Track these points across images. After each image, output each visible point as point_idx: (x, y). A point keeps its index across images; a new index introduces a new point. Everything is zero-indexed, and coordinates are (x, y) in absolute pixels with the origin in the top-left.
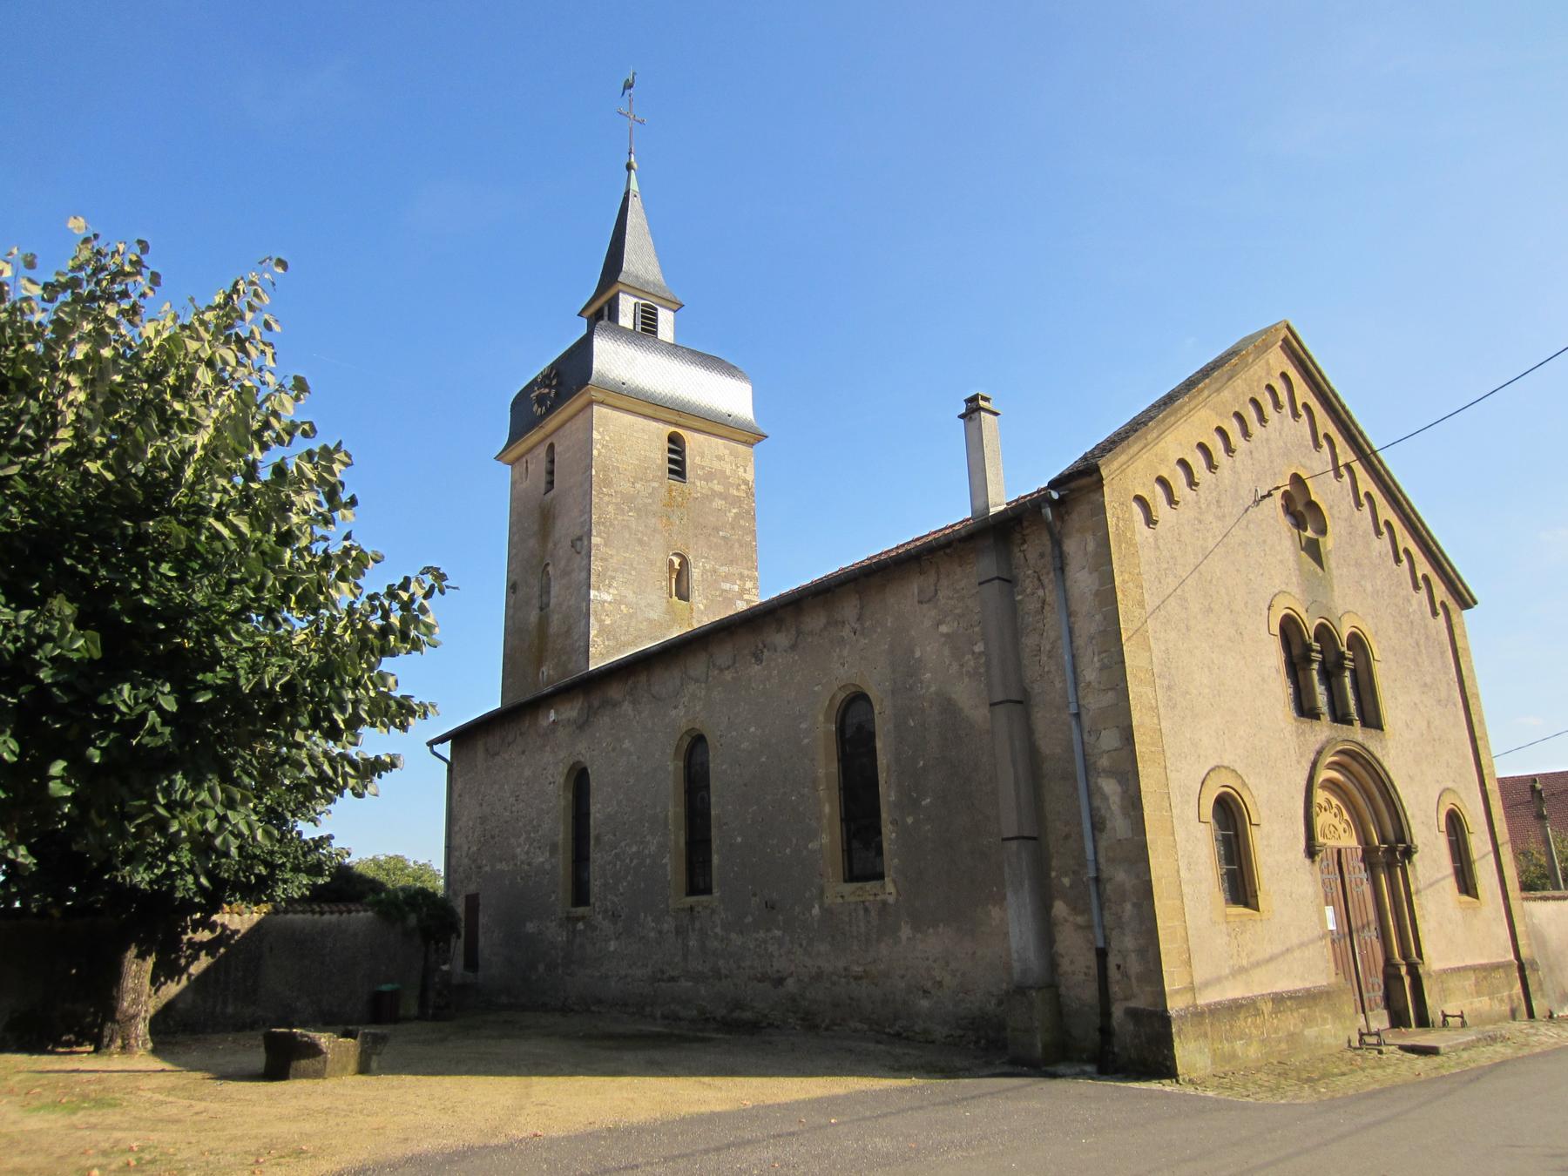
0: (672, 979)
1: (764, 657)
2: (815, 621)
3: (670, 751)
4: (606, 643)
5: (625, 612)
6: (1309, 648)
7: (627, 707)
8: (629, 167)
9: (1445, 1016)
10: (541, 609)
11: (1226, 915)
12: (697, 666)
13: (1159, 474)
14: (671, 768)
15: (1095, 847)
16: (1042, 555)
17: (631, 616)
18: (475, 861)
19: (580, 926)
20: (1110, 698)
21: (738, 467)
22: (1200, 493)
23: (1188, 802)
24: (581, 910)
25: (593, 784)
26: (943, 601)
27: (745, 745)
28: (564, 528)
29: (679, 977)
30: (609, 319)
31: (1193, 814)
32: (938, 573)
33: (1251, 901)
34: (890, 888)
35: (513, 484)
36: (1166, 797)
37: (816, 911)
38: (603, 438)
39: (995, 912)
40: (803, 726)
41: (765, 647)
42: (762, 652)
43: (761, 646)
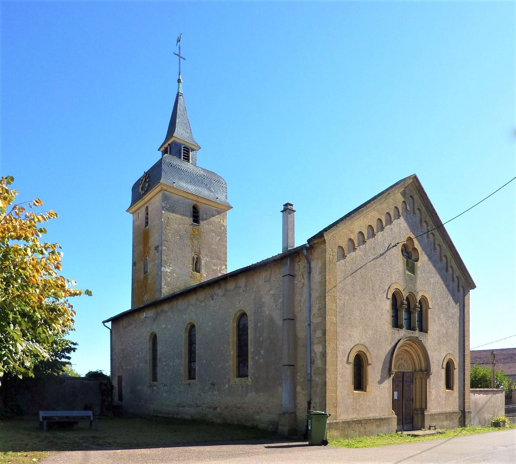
0: (183, 406)
1: (215, 298)
3: (184, 330)
4: (168, 288)
5: (175, 276)
6: (402, 304)
7: (169, 313)
8: (179, 81)
9: (430, 426)
10: (145, 273)
11: (446, 391)
12: (192, 299)
13: (350, 238)
14: (184, 336)
15: (311, 369)
16: (304, 267)
17: (178, 278)
19: (155, 388)
20: (319, 320)
21: (221, 220)
22: (367, 245)
23: (344, 356)
24: (155, 383)
25: (158, 340)
28: (153, 240)
29: (185, 406)
30: (170, 154)
32: (271, 271)
33: (364, 389)
34: (250, 380)
35: (134, 222)
36: (336, 354)
37: (227, 386)
38: (166, 206)
40: (226, 324)
41: (215, 294)
42: (214, 296)
43: (213, 294)
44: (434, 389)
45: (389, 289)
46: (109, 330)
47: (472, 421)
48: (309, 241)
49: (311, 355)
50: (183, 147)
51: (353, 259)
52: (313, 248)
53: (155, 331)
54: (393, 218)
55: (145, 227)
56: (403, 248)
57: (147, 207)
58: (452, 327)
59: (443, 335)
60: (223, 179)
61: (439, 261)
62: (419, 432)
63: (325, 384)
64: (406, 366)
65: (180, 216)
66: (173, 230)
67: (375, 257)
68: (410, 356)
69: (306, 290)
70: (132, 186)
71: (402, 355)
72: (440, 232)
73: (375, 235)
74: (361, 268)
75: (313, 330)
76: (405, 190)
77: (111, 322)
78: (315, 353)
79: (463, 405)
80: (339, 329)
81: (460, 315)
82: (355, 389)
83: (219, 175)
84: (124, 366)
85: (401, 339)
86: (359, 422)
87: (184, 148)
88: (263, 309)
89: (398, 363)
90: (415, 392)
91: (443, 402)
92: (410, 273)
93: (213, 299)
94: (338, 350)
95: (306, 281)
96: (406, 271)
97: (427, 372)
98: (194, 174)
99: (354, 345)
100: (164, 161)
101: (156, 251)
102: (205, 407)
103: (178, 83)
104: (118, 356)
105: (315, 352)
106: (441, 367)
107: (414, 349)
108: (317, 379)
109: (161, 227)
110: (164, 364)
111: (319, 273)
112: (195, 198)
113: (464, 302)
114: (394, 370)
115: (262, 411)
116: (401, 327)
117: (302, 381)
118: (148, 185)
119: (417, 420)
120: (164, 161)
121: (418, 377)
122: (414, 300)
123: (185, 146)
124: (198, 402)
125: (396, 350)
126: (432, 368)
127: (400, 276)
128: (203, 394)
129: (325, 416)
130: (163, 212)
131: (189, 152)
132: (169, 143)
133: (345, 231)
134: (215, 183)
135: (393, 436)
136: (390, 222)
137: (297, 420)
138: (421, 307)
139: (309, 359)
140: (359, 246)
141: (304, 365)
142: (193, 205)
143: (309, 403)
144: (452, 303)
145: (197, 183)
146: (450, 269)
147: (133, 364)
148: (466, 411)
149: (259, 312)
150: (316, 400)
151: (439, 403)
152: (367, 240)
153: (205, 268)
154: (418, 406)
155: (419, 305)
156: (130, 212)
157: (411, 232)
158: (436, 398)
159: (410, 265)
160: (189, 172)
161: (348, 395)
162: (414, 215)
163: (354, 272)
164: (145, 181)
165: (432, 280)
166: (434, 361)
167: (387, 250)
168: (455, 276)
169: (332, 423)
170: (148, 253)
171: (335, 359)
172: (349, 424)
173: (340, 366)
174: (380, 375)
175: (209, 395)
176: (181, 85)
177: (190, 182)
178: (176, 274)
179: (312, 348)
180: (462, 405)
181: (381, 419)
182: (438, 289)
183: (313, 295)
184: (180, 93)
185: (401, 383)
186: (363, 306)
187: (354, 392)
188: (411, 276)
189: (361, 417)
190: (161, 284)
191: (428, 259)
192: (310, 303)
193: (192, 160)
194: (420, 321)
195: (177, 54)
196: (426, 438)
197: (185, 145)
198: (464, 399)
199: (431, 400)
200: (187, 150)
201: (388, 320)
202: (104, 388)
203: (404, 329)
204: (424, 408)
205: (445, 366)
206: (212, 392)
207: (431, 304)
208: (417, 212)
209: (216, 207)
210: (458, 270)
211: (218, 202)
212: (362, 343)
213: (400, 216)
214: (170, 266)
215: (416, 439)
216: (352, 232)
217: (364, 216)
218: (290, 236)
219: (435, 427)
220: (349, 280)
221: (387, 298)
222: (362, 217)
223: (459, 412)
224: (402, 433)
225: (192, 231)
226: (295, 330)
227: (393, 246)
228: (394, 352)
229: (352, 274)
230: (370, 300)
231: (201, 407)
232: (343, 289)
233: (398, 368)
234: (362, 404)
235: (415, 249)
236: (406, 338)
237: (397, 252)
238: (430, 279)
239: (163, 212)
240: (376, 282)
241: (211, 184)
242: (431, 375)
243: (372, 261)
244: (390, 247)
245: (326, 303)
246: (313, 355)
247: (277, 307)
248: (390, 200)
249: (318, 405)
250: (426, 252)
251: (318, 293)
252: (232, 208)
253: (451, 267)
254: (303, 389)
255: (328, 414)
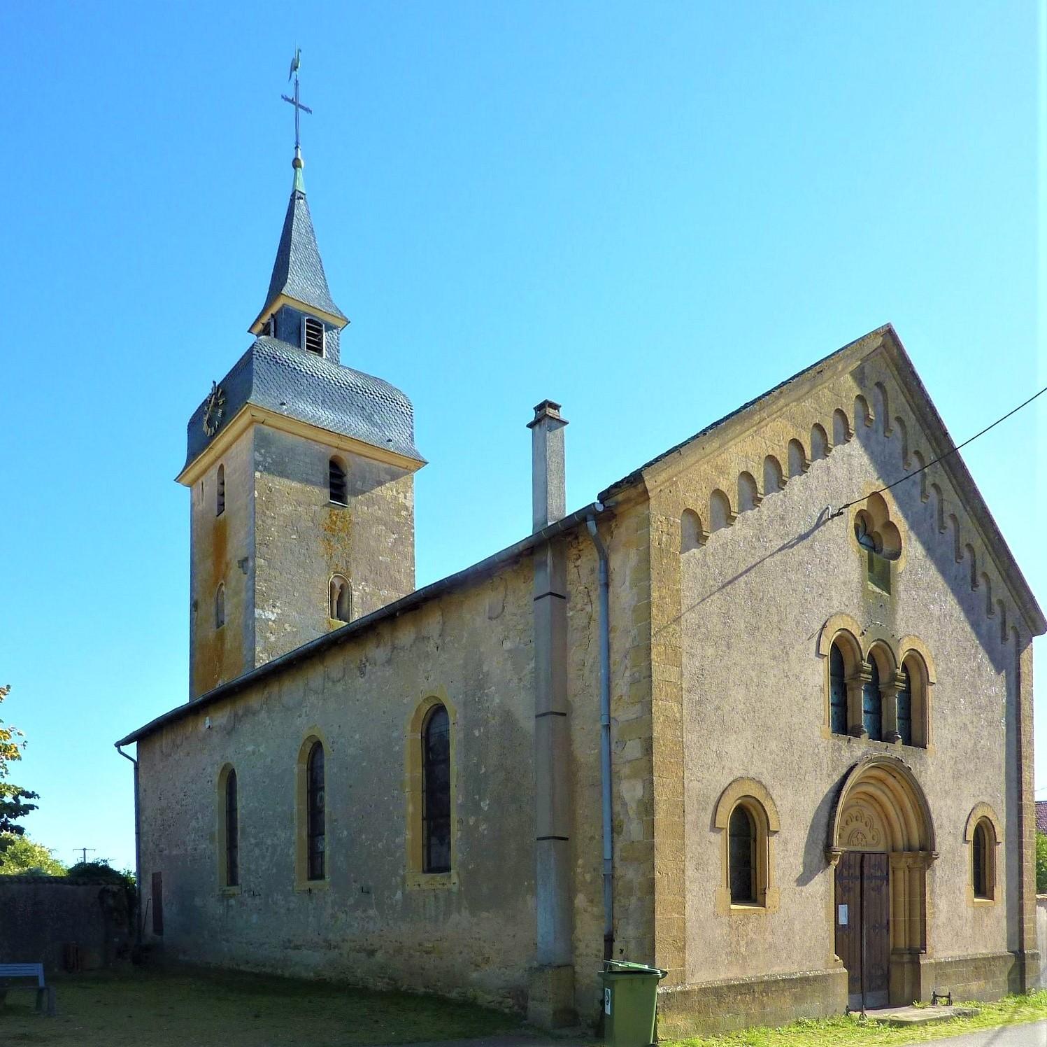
0: (297, 947)
2: (406, 635)
3: (296, 755)
6: (858, 669)
7: (263, 715)
8: (296, 164)
9: (935, 996)
11: (974, 902)
12: (315, 676)
13: (717, 487)
14: (296, 771)
15: (612, 848)
16: (592, 571)
18: (157, 845)
19: (232, 902)
22: (763, 509)
23: (705, 809)
24: (234, 889)
25: (239, 783)
26: (508, 618)
27: (351, 751)
28: (236, 547)
29: (301, 946)
30: (275, 336)
31: (707, 819)
33: (759, 898)
34: (455, 879)
35: (193, 505)
37: (399, 895)
38: (265, 460)
39: (530, 901)
42: (365, 667)
44: (944, 897)
45: (822, 629)
46: (132, 763)
47: (1041, 978)
48: (603, 496)
49: (611, 808)
50: (308, 321)
51: (724, 545)
52: (616, 515)
53: (231, 762)
54: (831, 440)
55: (218, 516)
56: (859, 523)
57: (222, 467)
58: (989, 733)
59: (966, 754)
60: (404, 395)
61: (954, 559)
62: (909, 1014)
63: (651, 887)
64: (869, 837)
65: (298, 485)
66: (282, 519)
67: (786, 542)
68: (879, 809)
69: (596, 632)
70: (189, 421)
71: (858, 808)
72: (955, 482)
73: (785, 484)
74: (746, 572)
75: (615, 741)
76: (863, 367)
77: (136, 742)
78: (625, 805)
79: (1019, 938)
80: (689, 738)
81: (1008, 702)
82: (735, 900)
83: (393, 385)
84: (166, 850)
85: (856, 764)
86: (746, 988)
87: (308, 324)
88: (486, 691)
89: (849, 829)
90: (894, 907)
91: (968, 931)
92: (878, 590)
93: (363, 674)
94: (686, 793)
95: (596, 608)
96: (869, 583)
97: (925, 851)
98: (332, 382)
99: (731, 779)
100: (257, 351)
101: (241, 569)
102: (349, 949)
103: (295, 168)
104: (151, 825)
105: (621, 798)
106: (960, 839)
107: (891, 790)
108: (629, 874)
109: (253, 513)
110: (253, 841)
111: (630, 583)
112: (335, 441)
113: (1019, 669)
114: (838, 848)
115: (487, 960)
116: (856, 733)
117: (589, 880)
118: (223, 414)
119: (900, 976)
120: (257, 351)
121: (902, 864)
122: (888, 661)
123: (310, 318)
124: (331, 936)
125: (844, 793)
126: (938, 840)
127: (852, 596)
128: (344, 916)
129: (650, 978)
130: (258, 474)
131: (320, 331)
132: (274, 313)
133: (702, 468)
134: (384, 404)
135: (838, 1025)
136: (823, 450)
137: (577, 986)
138: (908, 681)
139: (607, 817)
140: (741, 511)
141: (594, 838)
142: (329, 458)
143: (609, 940)
144: (989, 669)
145: (339, 404)
146: (981, 581)
147: (184, 842)
148: (1025, 952)
149: (477, 700)
150: (627, 932)
151: (957, 933)
152: (765, 495)
153: (361, 610)
154: (902, 942)
155: (904, 675)
156: (183, 482)
157: (880, 480)
158: (950, 920)
159: (877, 568)
160: (320, 377)
161: (716, 915)
162: (887, 434)
163: (730, 582)
164: (216, 405)
165: (935, 609)
166: (944, 822)
167: (817, 526)
168: (994, 600)
169: (672, 993)
170: (224, 577)
171: (679, 817)
172: (718, 994)
173: (691, 838)
174: (801, 860)
175: (357, 918)
176: (300, 171)
177: (323, 402)
178: (290, 626)
179: (615, 790)
180: (1017, 938)
181: (805, 981)
182: (952, 634)
183: (616, 645)
184: (300, 192)
185: (858, 883)
186: (753, 674)
187: (733, 907)
188: (882, 596)
189: (750, 974)
190: (255, 649)
191: (924, 553)
192: (609, 666)
193: (329, 353)
194: (906, 717)
195: (291, 98)
196: (931, 1029)
197: (310, 315)
198: (1021, 921)
199: (937, 925)
200: (316, 328)
201: (823, 712)
202: (111, 902)
203: (865, 737)
204: (919, 947)
205: (970, 836)
206: (365, 911)
207: (934, 672)
208: (895, 426)
209: (386, 462)
210: (1002, 584)
211: (392, 450)
212: (752, 774)
213: (850, 435)
214: (274, 607)
215: (904, 1033)
216: (722, 472)
217: (755, 428)
218: (552, 488)
219: (948, 997)
220: (715, 604)
221: (818, 654)
222: (748, 433)
223: (1010, 956)
224: (862, 1018)
225: (328, 521)
226: (568, 741)
227: (833, 516)
228: (839, 798)
229: (723, 587)
230: (774, 658)
231: (339, 948)
232: (699, 627)
233: (849, 843)
234: (752, 941)
235: (890, 526)
236: (871, 761)
237: (843, 530)
238: (932, 606)
239: (258, 474)
240: (788, 610)
241: (373, 406)
242: (936, 859)
243: (777, 552)
244: (824, 519)
245: (650, 664)
246: (617, 808)
247: (521, 685)
248: (825, 393)
249: (633, 945)
250: (919, 535)
251: (630, 639)
252: (427, 463)
253: (985, 575)
254: (592, 901)
255: (659, 971)
